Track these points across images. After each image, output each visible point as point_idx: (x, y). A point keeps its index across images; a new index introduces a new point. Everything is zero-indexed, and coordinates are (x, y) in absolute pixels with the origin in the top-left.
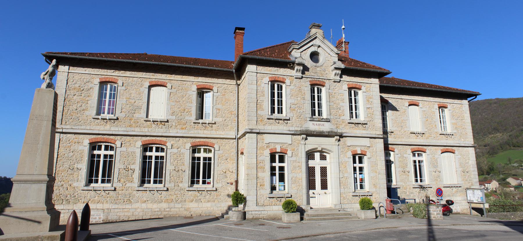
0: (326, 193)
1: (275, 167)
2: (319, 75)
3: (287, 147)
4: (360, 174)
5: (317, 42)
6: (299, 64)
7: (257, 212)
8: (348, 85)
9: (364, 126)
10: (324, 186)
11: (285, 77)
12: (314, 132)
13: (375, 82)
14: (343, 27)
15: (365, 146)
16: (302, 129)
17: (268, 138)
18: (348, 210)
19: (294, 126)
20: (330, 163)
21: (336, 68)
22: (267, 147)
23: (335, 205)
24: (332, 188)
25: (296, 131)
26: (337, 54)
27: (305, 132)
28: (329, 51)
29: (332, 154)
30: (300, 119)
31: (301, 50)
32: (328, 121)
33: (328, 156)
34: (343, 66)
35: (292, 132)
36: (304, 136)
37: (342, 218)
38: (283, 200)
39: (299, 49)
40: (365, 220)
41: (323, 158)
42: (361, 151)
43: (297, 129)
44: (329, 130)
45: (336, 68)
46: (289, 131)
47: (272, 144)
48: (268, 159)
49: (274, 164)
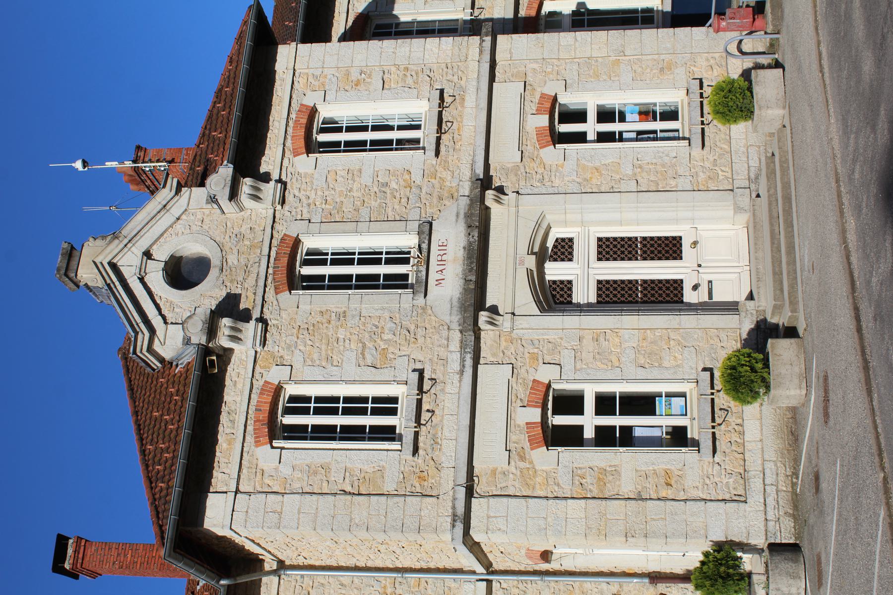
0: (695, 243)
1: (599, 429)
2: (253, 258)
3: (525, 384)
4: (622, 119)
5: (129, 263)
6: (212, 331)
7: (771, 501)
8: (296, 154)
9: (448, 100)
10: (668, 248)
11: (258, 385)
12: (467, 281)
13: (287, 56)
14: (78, 165)
15: (523, 98)
16: (456, 327)
17: (490, 454)
18: (754, 163)
19: (445, 353)
20: (586, 223)
21: (234, 194)
22: (522, 458)
23: (738, 209)
24: (677, 221)
25: (463, 345)
26: (178, 191)
27: (470, 314)
28: (166, 220)
29: (549, 218)
30: (420, 332)
31: (156, 321)
32: (426, 230)
33: (558, 232)
34: (226, 171)
35: (469, 362)
36: (483, 316)
37: (786, 186)
38: (723, 400)
39: (152, 331)
40: (789, 103)
41: (564, 250)
42: (539, 112)
43: (455, 345)
44: (461, 227)
45: (234, 194)
46: (462, 372)
47: (513, 437)
48: (568, 455)
49: (589, 433)
